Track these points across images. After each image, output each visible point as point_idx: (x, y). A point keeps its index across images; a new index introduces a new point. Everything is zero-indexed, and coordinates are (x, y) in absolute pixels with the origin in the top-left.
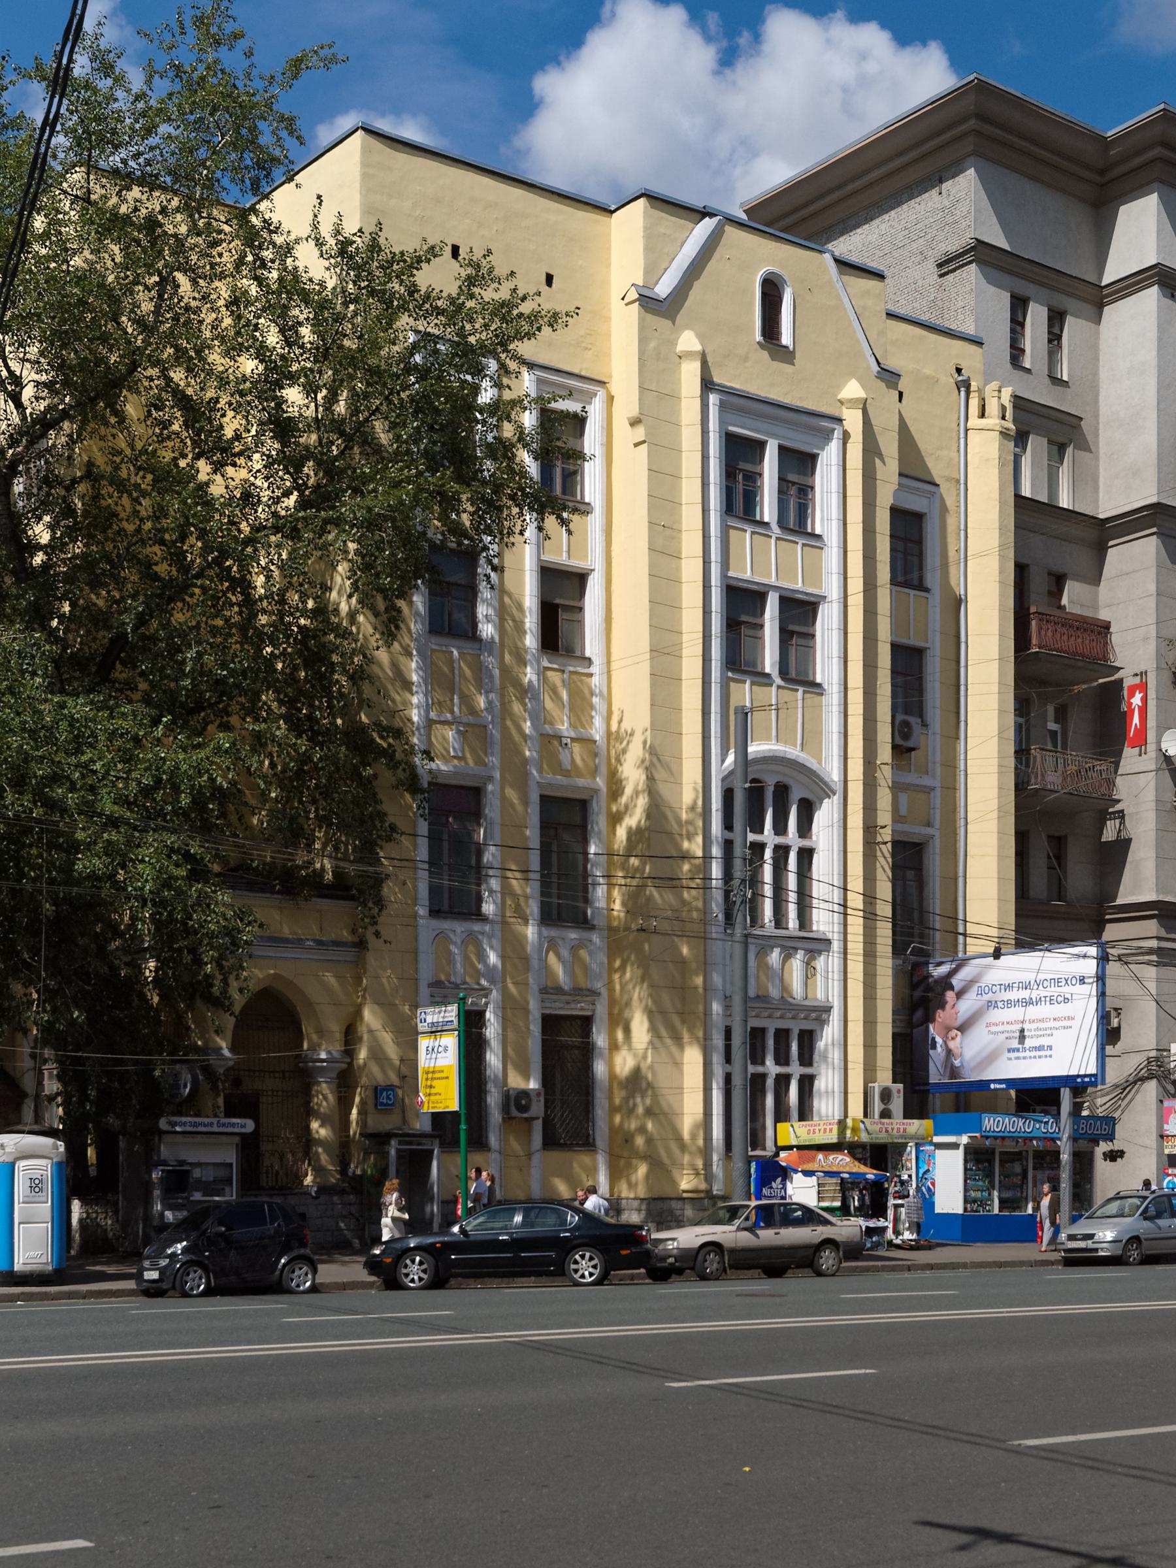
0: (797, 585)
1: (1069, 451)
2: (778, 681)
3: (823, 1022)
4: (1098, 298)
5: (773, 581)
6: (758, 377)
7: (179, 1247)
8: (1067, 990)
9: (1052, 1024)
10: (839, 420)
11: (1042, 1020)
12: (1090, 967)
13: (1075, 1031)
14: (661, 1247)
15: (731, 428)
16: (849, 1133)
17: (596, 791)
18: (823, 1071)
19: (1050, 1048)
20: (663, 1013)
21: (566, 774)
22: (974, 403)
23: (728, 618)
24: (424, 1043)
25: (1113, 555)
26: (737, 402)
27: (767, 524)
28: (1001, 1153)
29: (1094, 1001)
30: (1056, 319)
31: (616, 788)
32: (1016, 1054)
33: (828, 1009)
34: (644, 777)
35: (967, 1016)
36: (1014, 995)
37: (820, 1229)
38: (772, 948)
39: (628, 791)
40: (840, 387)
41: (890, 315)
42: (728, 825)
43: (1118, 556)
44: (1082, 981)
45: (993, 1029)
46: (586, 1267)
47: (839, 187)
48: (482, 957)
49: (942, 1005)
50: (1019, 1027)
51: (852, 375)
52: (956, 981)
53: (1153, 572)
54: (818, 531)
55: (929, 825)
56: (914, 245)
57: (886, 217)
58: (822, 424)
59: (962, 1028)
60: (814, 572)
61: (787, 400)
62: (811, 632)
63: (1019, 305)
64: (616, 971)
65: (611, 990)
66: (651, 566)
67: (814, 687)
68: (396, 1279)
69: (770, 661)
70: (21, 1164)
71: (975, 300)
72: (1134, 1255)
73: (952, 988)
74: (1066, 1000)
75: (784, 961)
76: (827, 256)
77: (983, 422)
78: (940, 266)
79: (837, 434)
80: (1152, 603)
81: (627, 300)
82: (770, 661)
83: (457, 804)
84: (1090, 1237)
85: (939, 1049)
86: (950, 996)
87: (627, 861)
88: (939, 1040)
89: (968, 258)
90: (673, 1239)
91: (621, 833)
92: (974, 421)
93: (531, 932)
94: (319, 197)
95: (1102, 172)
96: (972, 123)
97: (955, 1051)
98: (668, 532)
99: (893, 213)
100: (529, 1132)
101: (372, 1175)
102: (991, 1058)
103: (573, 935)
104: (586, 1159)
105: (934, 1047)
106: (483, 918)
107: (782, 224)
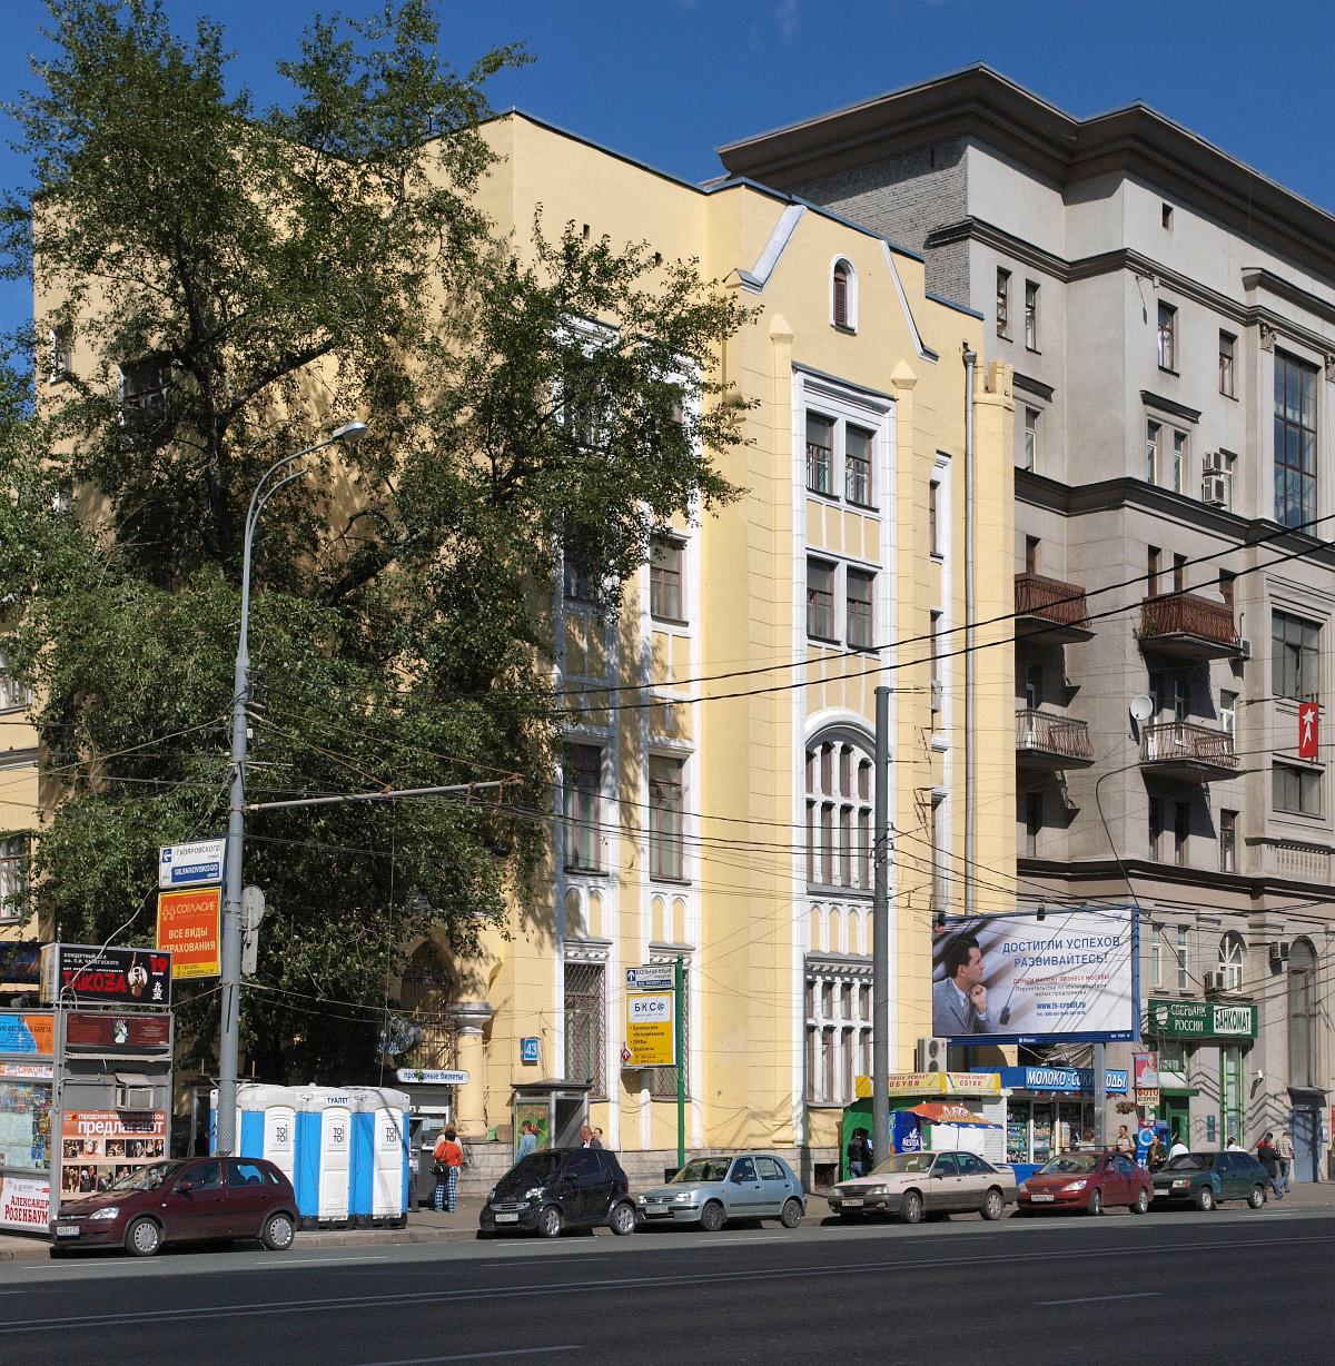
0: (863, 559)
6: (836, 358)
7: (537, 1192)
12: (1122, 929)
14: (869, 1193)
26: (820, 381)
28: (1035, 1105)
32: (1047, 1010)
37: (988, 1176)
56: (905, 212)
59: (989, 984)
60: (873, 547)
69: (840, 632)
72: (714, 1221)
73: (976, 944)
76: (883, 243)
81: (728, 282)
82: (840, 632)
86: (974, 952)
90: (883, 1186)
97: (980, 1006)
107: (756, 172)
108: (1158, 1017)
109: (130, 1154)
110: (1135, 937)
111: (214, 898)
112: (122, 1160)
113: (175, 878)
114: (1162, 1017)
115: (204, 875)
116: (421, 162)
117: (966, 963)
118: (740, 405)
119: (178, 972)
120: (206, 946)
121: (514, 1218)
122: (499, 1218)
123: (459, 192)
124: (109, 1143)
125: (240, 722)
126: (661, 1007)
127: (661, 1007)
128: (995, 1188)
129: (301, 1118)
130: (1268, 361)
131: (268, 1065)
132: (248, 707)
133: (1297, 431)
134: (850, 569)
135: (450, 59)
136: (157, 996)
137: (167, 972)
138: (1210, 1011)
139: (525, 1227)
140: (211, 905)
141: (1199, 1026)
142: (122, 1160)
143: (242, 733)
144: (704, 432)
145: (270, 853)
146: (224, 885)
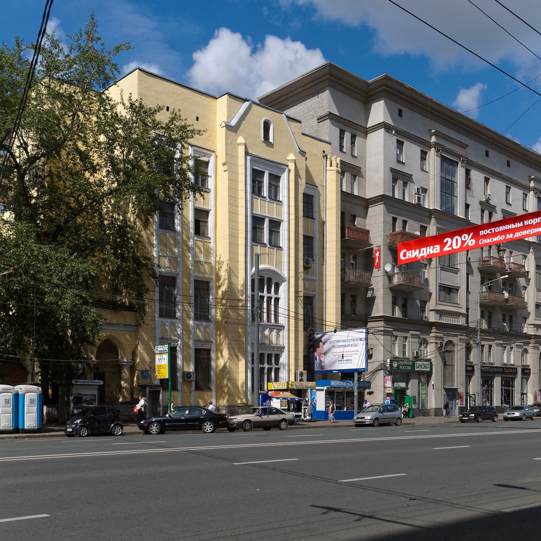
1: (357, 178)
2: (268, 246)
4: (366, 132)
5: (267, 215)
7: (79, 421)
8: (356, 342)
9: (352, 353)
10: (288, 166)
12: (363, 336)
15: (254, 167)
16: (290, 386)
17: (212, 279)
21: (203, 273)
22: (328, 162)
24: (157, 357)
26: (255, 159)
28: (337, 392)
30: (353, 137)
31: (218, 278)
33: (284, 348)
34: (227, 275)
37: (281, 415)
38: (266, 328)
39: (222, 279)
40: (288, 155)
42: (253, 290)
44: (361, 340)
45: (334, 354)
46: (208, 427)
47: (288, 94)
49: (319, 347)
50: (342, 354)
52: (323, 339)
55: (315, 291)
56: (311, 113)
57: (302, 104)
59: (325, 354)
60: (279, 212)
63: (342, 133)
70: (27, 394)
71: (329, 130)
74: (356, 346)
78: (318, 119)
80: (382, 225)
82: (266, 240)
83: (168, 282)
86: (321, 344)
88: (318, 357)
89: (327, 117)
91: (220, 292)
92: (328, 168)
93: (191, 322)
95: (367, 93)
98: (234, 199)
100: (191, 385)
102: (333, 363)
105: (316, 360)
107: (271, 104)
108: (394, 365)
110: (367, 339)
114: (395, 365)
117: (319, 347)
129: (17, 396)
130: (438, 159)
133: (450, 182)
134: (269, 220)
138: (414, 364)
141: (409, 368)
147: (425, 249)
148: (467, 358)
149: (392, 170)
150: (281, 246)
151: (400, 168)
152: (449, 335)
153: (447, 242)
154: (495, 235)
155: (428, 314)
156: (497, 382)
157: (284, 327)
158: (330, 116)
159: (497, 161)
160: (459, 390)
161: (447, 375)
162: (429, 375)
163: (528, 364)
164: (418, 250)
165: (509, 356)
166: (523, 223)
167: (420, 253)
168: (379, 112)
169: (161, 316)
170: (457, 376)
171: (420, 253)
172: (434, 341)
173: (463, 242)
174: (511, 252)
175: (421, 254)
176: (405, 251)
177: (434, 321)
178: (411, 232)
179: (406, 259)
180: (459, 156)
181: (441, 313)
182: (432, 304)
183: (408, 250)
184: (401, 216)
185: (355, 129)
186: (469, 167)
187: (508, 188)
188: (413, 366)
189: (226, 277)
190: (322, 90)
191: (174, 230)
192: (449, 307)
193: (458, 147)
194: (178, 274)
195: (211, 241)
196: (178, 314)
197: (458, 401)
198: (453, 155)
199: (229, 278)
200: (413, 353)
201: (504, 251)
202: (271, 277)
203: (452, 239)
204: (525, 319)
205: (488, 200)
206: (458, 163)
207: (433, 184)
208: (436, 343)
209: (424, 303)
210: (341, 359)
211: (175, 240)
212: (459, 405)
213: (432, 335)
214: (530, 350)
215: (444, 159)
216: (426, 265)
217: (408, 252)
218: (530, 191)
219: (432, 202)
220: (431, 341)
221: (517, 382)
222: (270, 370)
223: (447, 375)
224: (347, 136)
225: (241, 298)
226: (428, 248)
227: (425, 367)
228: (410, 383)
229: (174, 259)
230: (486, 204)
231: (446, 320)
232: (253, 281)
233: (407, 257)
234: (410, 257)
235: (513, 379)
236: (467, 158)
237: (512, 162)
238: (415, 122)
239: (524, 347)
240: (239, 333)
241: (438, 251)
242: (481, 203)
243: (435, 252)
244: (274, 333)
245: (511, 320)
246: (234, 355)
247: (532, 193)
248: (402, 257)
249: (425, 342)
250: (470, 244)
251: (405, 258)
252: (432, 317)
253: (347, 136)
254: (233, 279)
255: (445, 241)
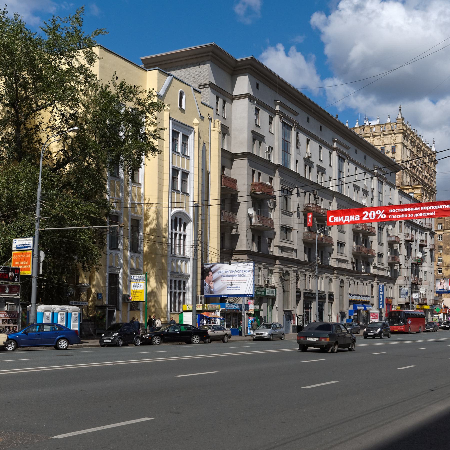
1: (226, 135)
2: (181, 193)
3: (188, 279)
4: (233, 98)
5: (180, 167)
7: (116, 334)
8: (245, 273)
9: (240, 281)
10: (193, 128)
11: (237, 280)
13: (247, 284)
16: (205, 308)
17: (142, 218)
18: (187, 292)
19: (240, 287)
20: (158, 276)
22: (212, 124)
23: (222, 188)
24: (132, 284)
25: (235, 162)
27: (179, 153)
29: (252, 277)
30: (224, 102)
31: (146, 217)
33: (189, 276)
34: (156, 216)
35: (216, 278)
36: (229, 274)
39: (151, 219)
40: (193, 120)
41: (202, 103)
42: (172, 229)
43: (236, 163)
44: (249, 271)
45: (223, 282)
46: (196, 339)
47: (170, 60)
48: (119, 261)
49: (208, 275)
50: (231, 282)
51: (195, 117)
52: (212, 269)
53: (246, 168)
54: (188, 155)
57: (183, 70)
58: (190, 129)
59: (214, 281)
60: (188, 166)
61: (183, 122)
62: (186, 180)
63: (217, 98)
64: (145, 265)
65: (144, 269)
66: (158, 162)
67: (188, 195)
68: (151, 342)
70: (73, 313)
71: (208, 95)
73: (211, 271)
74: (244, 276)
75: (181, 263)
77: (214, 129)
78: (199, 86)
79: (193, 132)
80: (246, 176)
84: (263, 334)
85: (207, 286)
86: (210, 273)
87: (149, 237)
88: (207, 284)
89: (208, 86)
91: (148, 229)
92: (212, 128)
93: (128, 254)
94: (115, 72)
95: (234, 68)
96: (211, 53)
97: (212, 287)
99: (185, 69)
100: (127, 306)
101: (99, 317)
102: (223, 289)
103: (137, 255)
104: (137, 312)
105: (206, 285)
106: (119, 250)
109: (9, 323)
111: (29, 253)
112: (7, 325)
113: (17, 248)
115: (27, 247)
116: (77, 57)
118: (162, 129)
119: (22, 273)
120: (27, 267)
121: (110, 341)
122: (105, 341)
123: (87, 66)
124: (3, 320)
125: (38, 207)
126: (141, 286)
127: (141, 286)
128: (226, 334)
130: (280, 124)
131: (42, 300)
132: (41, 202)
134: (182, 172)
135: (86, 31)
136: (16, 280)
137: (19, 273)
138: (265, 289)
139: (112, 344)
140: (29, 255)
142: (7, 325)
143: (39, 209)
144: (151, 135)
145: (45, 242)
146: (33, 250)
147: (348, 217)
148: (297, 287)
149: (253, 132)
150: (188, 193)
151: (257, 130)
152: (287, 267)
153: (365, 214)
154: (401, 213)
155: (273, 249)
156: (314, 306)
157: (190, 259)
158: (211, 85)
159: (313, 126)
160: (292, 312)
161: (286, 300)
162: (274, 299)
163: (332, 291)
164: (343, 217)
165: (321, 285)
166: (420, 208)
167: (344, 219)
168: (243, 85)
169: (110, 249)
170: (291, 300)
171: (344, 219)
172: (278, 271)
173: (377, 216)
174: (322, 199)
175: (346, 220)
176: (333, 216)
177: (278, 255)
178: (264, 182)
179: (333, 223)
180: (293, 122)
181: (282, 248)
182: (276, 241)
183: (336, 216)
184: (258, 169)
185: (225, 96)
186: (298, 131)
187: (321, 148)
188: (265, 292)
189: (155, 216)
190: (204, 63)
191: (120, 178)
192: (287, 244)
193: (293, 115)
194: (121, 214)
195: (142, 186)
196: (120, 247)
197: (292, 321)
198: (287, 119)
199: (157, 218)
200: (265, 282)
201: (318, 198)
202: (181, 217)
203: (369, 212)
204: (330, 254)
205: (309, 157)
206: (291, 127)
207: (277, 144)
208: (279, 273)
209: (271, 240)
210: (230, 286)
211: (120, 186)
212: (292, 325)
213: (276, 266)
214: (375, 285)
215: (284, 124)
216: (271, 209)
217: (335, 218)
218: (333, 150)
219: (276, 160)
220: (275, 271)
221: (326, 305)
222: (180, 293)
223: (286, 300)
224: (220, 101)
225: (164, 234)
226: (351, 216)
227: (272, 293)
228: (262, 305)
229: (119, 202)
230: (308, 161)
231: (286, 255)
232: (172, 220)
233: (335, 221)
234: (337, 221)
235: (324, 302)
236: (298, 124)
237: (323, 127)
238: (268, 96)
239: (330, 277)
240: (163, 263)
241: (359, 219)
242: (305, 159)
243: (356, 219)
244: (184, 263)
245: (322, 255)
246: (159, 281)
247: (335, 152)
248: (330, 220)
249: (271, 272)
250: (382, 217)
251: (332, 222)
252: (276, 252)
253: (220, 101)
254: (160, 221)
255: (364, 213)
